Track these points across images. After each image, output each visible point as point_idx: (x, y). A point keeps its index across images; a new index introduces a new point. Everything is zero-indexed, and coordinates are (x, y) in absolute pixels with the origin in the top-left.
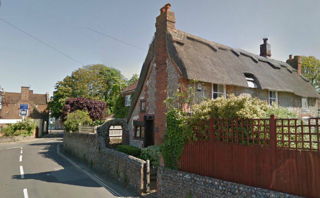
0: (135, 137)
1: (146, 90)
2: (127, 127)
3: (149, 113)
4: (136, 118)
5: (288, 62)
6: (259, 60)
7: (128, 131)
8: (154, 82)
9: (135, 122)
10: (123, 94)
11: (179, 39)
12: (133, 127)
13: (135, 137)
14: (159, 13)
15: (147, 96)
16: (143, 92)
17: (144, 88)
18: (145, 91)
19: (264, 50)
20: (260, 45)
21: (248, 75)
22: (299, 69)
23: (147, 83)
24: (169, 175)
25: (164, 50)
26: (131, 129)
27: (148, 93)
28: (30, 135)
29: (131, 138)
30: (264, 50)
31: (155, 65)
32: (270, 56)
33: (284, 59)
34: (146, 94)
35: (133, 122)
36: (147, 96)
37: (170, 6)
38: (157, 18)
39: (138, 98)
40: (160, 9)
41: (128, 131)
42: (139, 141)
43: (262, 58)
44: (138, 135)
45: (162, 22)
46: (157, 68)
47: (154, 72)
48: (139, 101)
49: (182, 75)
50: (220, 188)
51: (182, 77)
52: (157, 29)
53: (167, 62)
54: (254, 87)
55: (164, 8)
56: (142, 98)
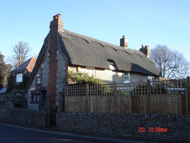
0: (32, 102)
1: (42, 70)
2: (26, 96)
3: (43, 86)
4: (33, 89)
5: (140, 50)
6: (119, 50)
7: (27, 98)
8: (48, 65)
9: (32, 91)
10: (15, 73)
11: (159, 130)
12: (31, 95)
13: (32, 102)
14: (52, 19)
15: (42, 74)
16: (39, 72)
17: (40, 69)
18: (40, 71)
19: (122, 42)
20: (120, 39)
21: (111, 61)
22: (148, 55)
23: (42, 66)
24: (64, 114)
25: (55, 42)
26: (28, 97)
27: (43, 72)
28: (85, 72)
29: (29, 103)
30: (122, 42)
31: (48, 54)
32: (127, 46)
33: (138, 48)
34: (41, 73)
35: (30, 92)
36: (42, 74)
37: (60, 15)
38: (51, 22)
39: (35, 75)
40: (53, 16)
41: (27, 98)
42: (35, 104)
43: (121, 48)
44: (35, 100)
45: (54, 24)
46: (49, 57)
47: (48, 59)
48: (35, 78)
49: (68, 62)
50: (91, 115)
51: (68, 63)
52: (50, 29)
53: (57, 52)
54: (114, 69)
55: (56, 16)
56: (38, 75)
